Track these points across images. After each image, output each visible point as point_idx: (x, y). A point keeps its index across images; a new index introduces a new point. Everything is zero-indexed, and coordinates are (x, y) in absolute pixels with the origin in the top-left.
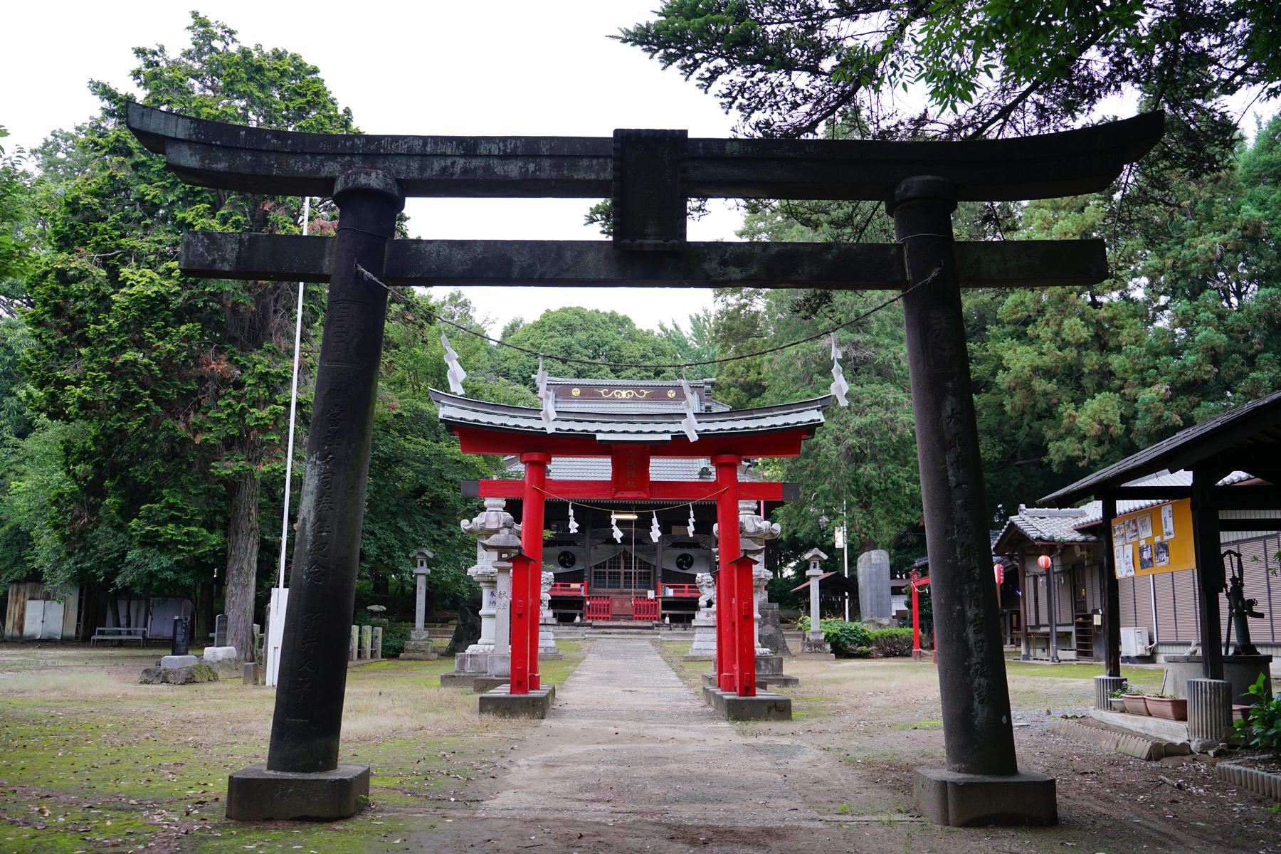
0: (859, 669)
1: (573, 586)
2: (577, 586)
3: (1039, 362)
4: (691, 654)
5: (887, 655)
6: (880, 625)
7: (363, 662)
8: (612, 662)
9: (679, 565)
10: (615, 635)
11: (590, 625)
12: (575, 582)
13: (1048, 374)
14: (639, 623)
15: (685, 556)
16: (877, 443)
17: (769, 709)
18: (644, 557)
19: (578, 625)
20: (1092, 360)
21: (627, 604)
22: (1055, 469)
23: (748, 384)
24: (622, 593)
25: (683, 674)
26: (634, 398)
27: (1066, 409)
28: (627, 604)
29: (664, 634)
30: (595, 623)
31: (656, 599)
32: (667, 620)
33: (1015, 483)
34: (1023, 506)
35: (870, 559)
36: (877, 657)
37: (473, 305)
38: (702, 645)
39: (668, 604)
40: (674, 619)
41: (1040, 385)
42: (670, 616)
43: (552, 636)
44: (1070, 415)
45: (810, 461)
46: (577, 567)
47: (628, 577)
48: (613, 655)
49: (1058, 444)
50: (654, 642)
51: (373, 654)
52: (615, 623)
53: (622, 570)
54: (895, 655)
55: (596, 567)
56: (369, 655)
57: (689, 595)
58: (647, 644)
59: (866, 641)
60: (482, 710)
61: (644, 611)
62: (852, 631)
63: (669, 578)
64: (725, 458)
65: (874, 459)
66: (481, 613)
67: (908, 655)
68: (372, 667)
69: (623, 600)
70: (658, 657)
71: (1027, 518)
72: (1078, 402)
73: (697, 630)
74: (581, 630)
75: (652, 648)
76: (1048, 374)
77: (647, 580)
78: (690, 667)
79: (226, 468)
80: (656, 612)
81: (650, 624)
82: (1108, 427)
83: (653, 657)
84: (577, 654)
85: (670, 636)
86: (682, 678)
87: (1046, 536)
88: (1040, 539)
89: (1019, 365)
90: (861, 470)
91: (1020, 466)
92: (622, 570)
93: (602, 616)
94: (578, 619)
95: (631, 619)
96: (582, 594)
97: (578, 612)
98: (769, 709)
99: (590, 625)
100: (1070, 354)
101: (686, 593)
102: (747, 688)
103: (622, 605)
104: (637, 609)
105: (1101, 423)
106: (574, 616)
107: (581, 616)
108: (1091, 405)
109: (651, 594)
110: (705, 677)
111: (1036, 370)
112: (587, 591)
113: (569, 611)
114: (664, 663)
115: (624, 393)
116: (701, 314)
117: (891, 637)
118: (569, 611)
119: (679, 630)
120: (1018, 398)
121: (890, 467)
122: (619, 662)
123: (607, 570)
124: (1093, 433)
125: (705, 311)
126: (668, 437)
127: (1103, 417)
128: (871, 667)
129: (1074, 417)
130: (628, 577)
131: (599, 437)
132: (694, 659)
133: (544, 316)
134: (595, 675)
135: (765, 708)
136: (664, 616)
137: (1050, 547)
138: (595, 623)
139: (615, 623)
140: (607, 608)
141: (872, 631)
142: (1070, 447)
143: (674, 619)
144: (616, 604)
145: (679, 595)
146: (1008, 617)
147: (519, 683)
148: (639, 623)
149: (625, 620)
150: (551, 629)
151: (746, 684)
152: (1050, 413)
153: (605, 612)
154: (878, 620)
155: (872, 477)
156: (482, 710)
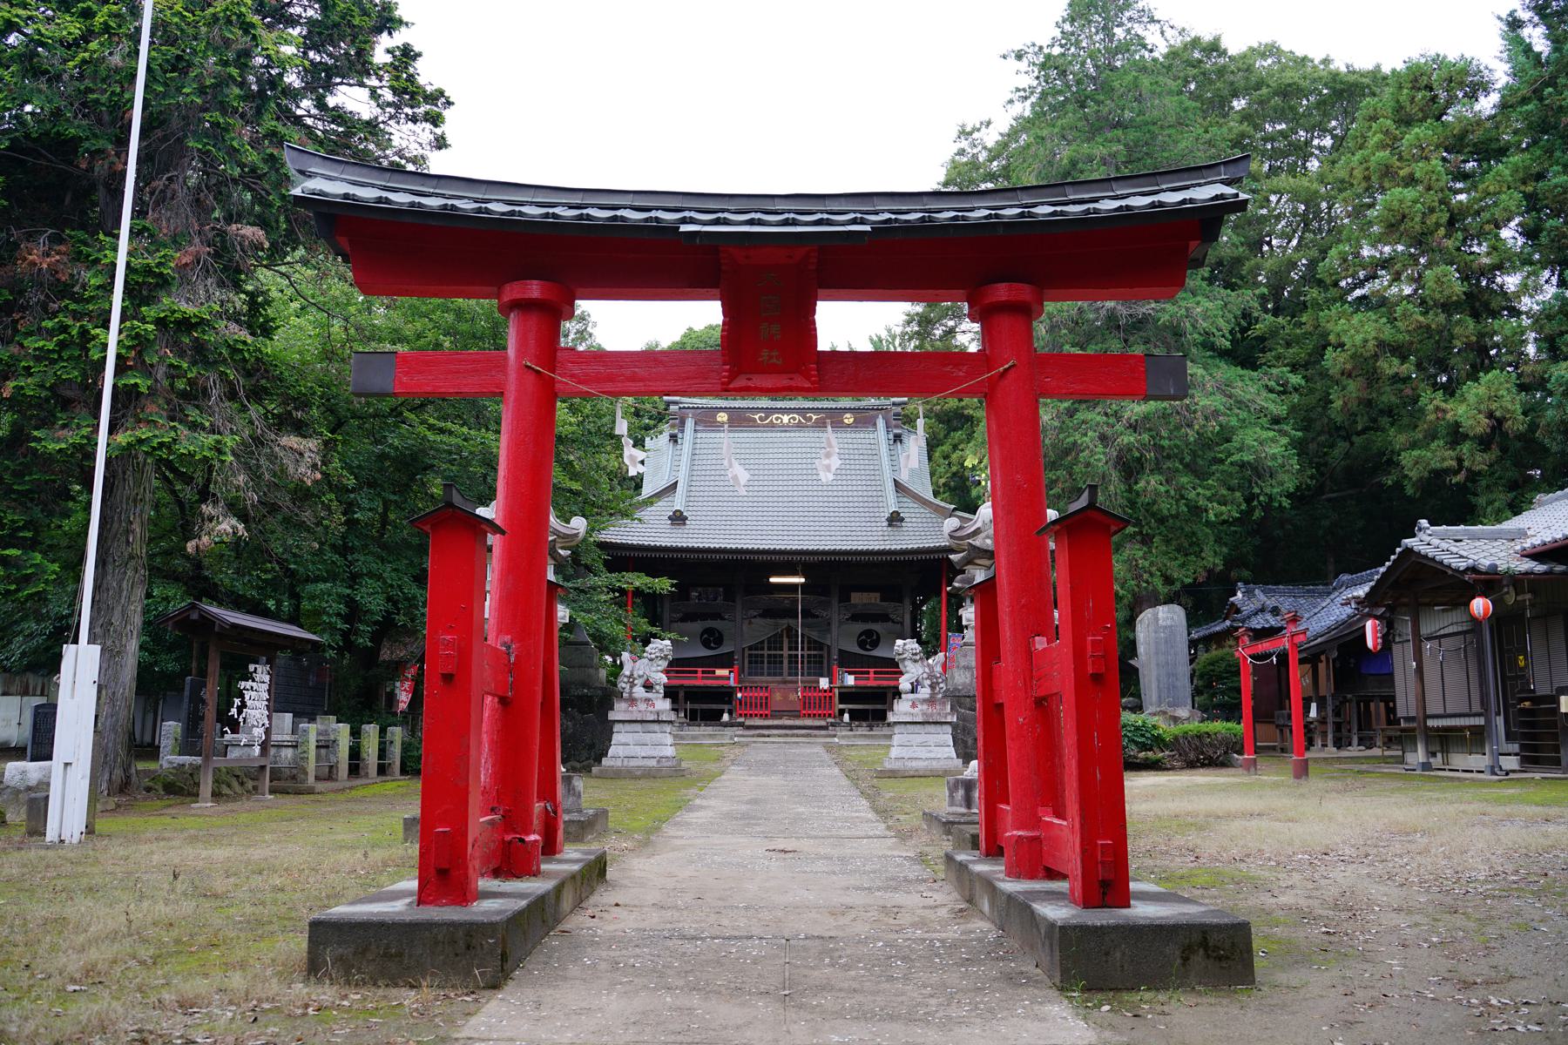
0: (1188, 791)
1: (719, 672)
2: (725, 672)
3: (1388, 334)
4: (888, 766)
5: (1191, 765)
6: (1175, 720)
7: (358, 782)
8: (763, 779)
9: (862, 645)
10: (776, 738)
11: (741, 725)
12: (722, 667)
13: (1400, 351)
14: (809, 722)
15: (868, 633)
16: (1165, 443)
17: (1187, 954)
18: (814, 635)
19: (726, 725)
20: (1466, 328)
21: (792, 697)
22: (1409, 491)
23: (946, 413)
24: (785, 682)
25: (881, 802)
26: (799, 425)
27: (1431, 401)
28: (792, 697)
29: (842, 737)
30: (749, 722)
31: (831, 689)
32: (846, 717)
33: (1326, 523)
34: (1424, 523)
35: (1157, 619)
36: (1173, 769)
37: (592, 319)
38: (905, 753)
39: (847, 696)
40: (855, 716)
41: (1390, 366)
42: (851, 712)
43: (669, 740)
44: (1437, 409)
45: (1061, 473)
46: (724, 649)
47: (793, 659)
48: (766, 768)
49: (1416, 453)
50: (829, 748)
51: (382, 770)
52: (776, 722)
53: (786, 652)
54: (1203, 766)
55: (750, 648)
56: (373, 770)
57: (874, 684)
58: (819, 750)
59: (1159, 742)
60: (314, 968)
61: (816, 708)
62: (1137, 728)
63: (848, 661)
64: (1002, 292)
65: (1157, 469)
66: (612, 716)
67: (1223, 765)
68: (377, 789)
69: (787, 692)
70: (836, 771)
71: (1435, 541)
72: (1450, 390)
73: (897, 729)
74: (729, 731)
75: (826, 756)
76: (1400, 351)
77: (818, 666)
78: (890, 790)
79: (59, 440)
80: (831, 706)
81: (823, 723)
82: (1500, 422)
83: (827, 771)
84: (712, 767)
85: (854, 740)
86: (883, 813)
87: (1485, 563)
88: (1473, 569)
89: (1359, 338)
90: (1142, 484)
91: (1329, 500)
92: (786, 652)
93: (759, 712)
94: (726, 717)
95: (798, 717)
96: (732, 683)
97: (726, 707)
98: (1187, 954)
99: (741, 725)
100: (1437, 319)
101: (872, 680)
102: (1105, 884)
103: (785, 698)
104: (806, 702)
105: (1490, 415)
106: (722, 712)
107: (730, 713)
108: (1474, 391)
109: (824, 683)
110: (930, 818)
111: (1381, 344)
112: (737, 680)
113: (714, 706)
114: (845, 782)
115: (786, 419)
116: (884, 335)
117: (1199, 736)
118: (714, 706)
119: (863, 731)
120: (1353, 387)
121: (1184, 480)
122: (775, 780)
123: (766, 652)
124: (1479, 430)
125: (889, 331)
126: (867, 228)
127: (1494, 406)
128: (1212, 789)
129: (1444, 411)
130: (793, 659)
131: (684, 228)
132: (893, 774)
133: (685, 336)
134: (726, 808)
135: (1173, 951)
136: (842, 712)
137: (1488, 581)
138: (749, 722)
139: (776, 722)
140: (765, 703)
141: (1166, 729)
142: (1439, 456)
143: (855, 716)
144: (778, 696)
145: (862, 683)
146: (1354, 704)
147: (443, 873)
148: (809, 722)
149: (790, 717)
150: (668, 728)
151: (1101, 873)
152: (1405, 411)
153: (763, 708)
154: (1170, 711)
155: (1158, 494)
156: (314, 968)
